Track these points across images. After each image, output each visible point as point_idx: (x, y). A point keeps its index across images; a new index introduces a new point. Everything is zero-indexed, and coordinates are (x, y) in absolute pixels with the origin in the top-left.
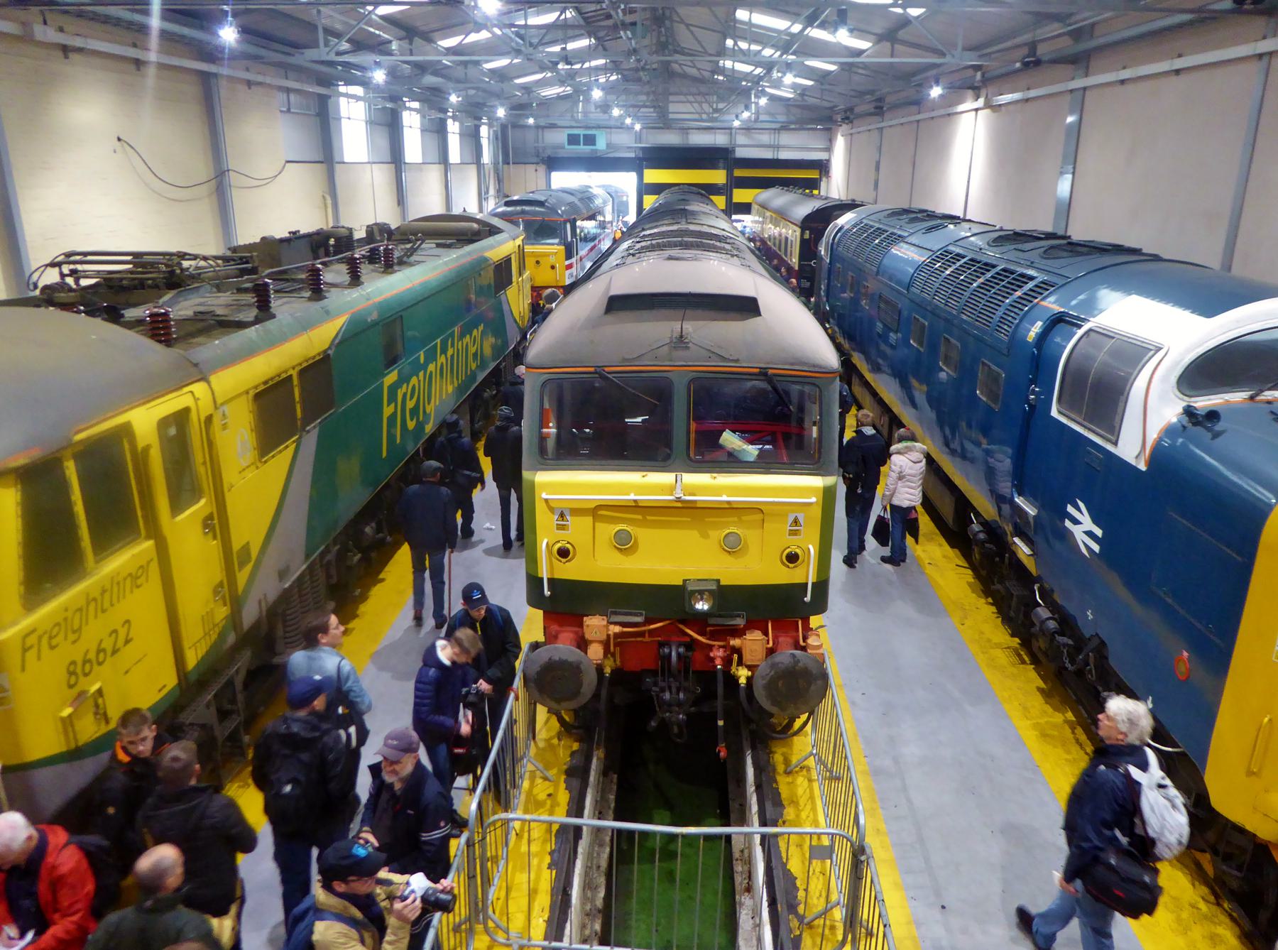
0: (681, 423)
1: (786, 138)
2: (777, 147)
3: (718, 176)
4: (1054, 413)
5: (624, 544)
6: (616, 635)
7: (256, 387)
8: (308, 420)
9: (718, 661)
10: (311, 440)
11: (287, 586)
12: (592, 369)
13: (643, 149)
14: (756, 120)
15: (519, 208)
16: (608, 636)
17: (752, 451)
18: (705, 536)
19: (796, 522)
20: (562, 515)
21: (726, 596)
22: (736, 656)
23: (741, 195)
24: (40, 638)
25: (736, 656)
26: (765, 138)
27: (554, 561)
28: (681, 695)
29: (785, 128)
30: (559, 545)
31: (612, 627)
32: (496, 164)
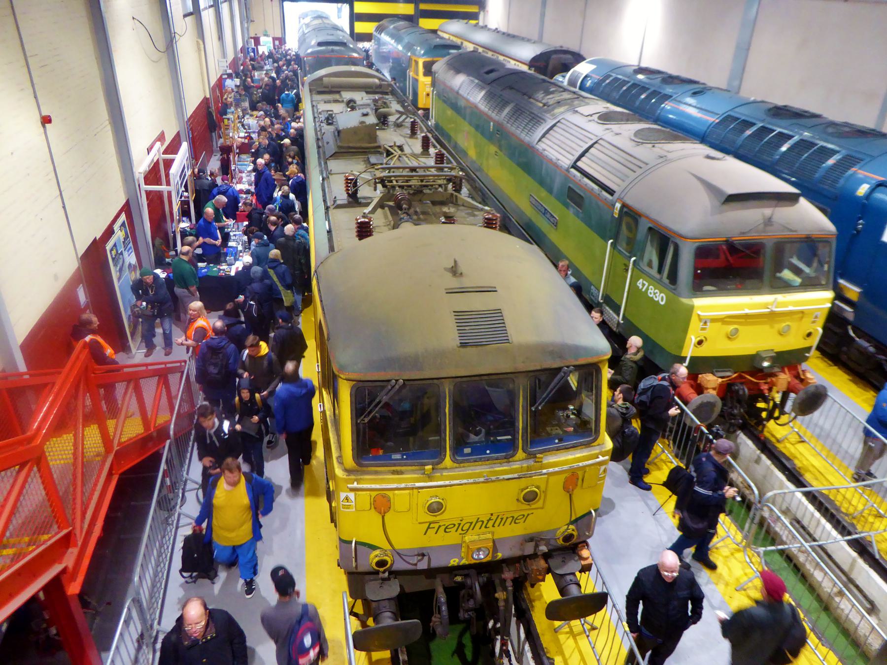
18: (772, 327)
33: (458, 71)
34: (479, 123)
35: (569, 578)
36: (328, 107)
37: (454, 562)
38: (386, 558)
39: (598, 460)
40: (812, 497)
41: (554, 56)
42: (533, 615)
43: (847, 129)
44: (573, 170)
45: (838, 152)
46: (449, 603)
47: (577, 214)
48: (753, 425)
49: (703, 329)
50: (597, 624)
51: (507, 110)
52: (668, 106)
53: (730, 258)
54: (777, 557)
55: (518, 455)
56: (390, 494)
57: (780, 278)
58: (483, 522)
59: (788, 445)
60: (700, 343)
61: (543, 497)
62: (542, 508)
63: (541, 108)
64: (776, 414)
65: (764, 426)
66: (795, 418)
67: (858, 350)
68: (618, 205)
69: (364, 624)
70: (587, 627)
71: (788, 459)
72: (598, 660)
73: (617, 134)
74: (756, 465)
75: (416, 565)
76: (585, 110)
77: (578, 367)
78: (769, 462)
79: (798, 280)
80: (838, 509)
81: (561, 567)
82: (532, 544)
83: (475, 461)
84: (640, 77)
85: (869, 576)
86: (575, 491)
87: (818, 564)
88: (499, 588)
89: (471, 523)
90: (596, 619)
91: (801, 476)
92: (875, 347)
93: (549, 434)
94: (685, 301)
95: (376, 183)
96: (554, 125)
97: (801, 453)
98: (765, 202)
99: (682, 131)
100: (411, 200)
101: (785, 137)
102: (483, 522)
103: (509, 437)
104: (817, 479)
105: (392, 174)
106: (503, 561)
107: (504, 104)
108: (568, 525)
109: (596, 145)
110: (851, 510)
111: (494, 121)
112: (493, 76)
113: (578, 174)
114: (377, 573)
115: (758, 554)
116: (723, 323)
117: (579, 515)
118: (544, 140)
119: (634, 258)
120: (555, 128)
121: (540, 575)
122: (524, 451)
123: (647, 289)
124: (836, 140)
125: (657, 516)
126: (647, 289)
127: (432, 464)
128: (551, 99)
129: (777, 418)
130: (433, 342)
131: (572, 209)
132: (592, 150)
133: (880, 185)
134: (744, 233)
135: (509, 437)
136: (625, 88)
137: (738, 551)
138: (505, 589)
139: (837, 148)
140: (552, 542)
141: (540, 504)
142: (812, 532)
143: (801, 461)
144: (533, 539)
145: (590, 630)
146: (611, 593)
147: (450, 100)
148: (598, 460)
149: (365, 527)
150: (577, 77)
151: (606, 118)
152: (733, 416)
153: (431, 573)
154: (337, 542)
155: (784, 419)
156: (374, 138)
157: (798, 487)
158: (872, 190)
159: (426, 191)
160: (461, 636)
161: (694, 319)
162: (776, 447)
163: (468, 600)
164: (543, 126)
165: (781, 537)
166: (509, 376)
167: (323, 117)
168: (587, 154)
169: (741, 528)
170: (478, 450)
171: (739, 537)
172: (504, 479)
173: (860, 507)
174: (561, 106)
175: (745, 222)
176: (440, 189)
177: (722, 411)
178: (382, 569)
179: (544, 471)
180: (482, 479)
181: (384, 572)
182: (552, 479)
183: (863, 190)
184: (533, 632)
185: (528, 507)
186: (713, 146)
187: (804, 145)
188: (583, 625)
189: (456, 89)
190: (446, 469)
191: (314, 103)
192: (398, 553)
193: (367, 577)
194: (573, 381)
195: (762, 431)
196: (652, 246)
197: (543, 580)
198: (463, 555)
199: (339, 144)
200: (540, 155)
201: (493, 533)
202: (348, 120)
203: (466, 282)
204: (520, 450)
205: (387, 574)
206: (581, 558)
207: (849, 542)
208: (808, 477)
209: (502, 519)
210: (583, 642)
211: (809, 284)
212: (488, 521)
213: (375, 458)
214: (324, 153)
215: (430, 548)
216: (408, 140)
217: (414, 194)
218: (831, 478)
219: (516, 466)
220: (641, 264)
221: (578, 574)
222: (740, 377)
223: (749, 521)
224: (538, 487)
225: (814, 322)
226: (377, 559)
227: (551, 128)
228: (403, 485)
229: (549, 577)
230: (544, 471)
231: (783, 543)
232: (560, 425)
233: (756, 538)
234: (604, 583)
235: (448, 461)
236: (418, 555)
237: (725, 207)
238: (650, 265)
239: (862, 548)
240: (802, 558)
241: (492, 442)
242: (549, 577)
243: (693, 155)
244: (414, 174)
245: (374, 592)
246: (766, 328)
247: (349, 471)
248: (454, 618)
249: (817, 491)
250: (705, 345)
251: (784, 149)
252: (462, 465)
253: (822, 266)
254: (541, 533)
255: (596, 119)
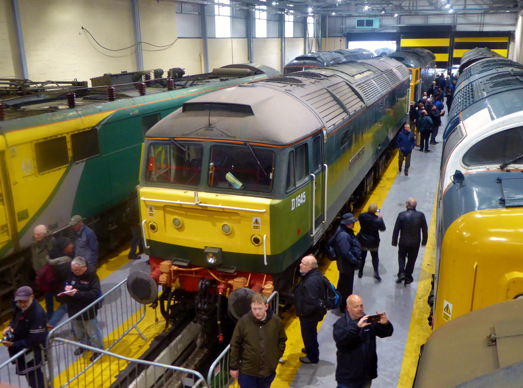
0: (209, 166)
1: (488, 19)
2: (482, 24)
3: (445, 42)
5: (179, 227)
6: (174, 271)
7: (38, 140)
8: (77, 157)
9: (221, 290)
10: (79, 168)
11: (55, 232)
12: (168, 139)
13: (400, 27)
14: (465, 9)
15: (302, 61)
16: (170, 271)
17: (239, 184)
18: (214, 225)
19: (256, 222)
20: (151, 209)
21: (224, 257)
22: (228, 289)
23: (457, 53)
25: (228, 289)
26: (475, 19)
27: (150, 231)
28: (206, 306)
29: (486, 13)
30: (151, 223)
31: (173, 267)
32: (317, 38)
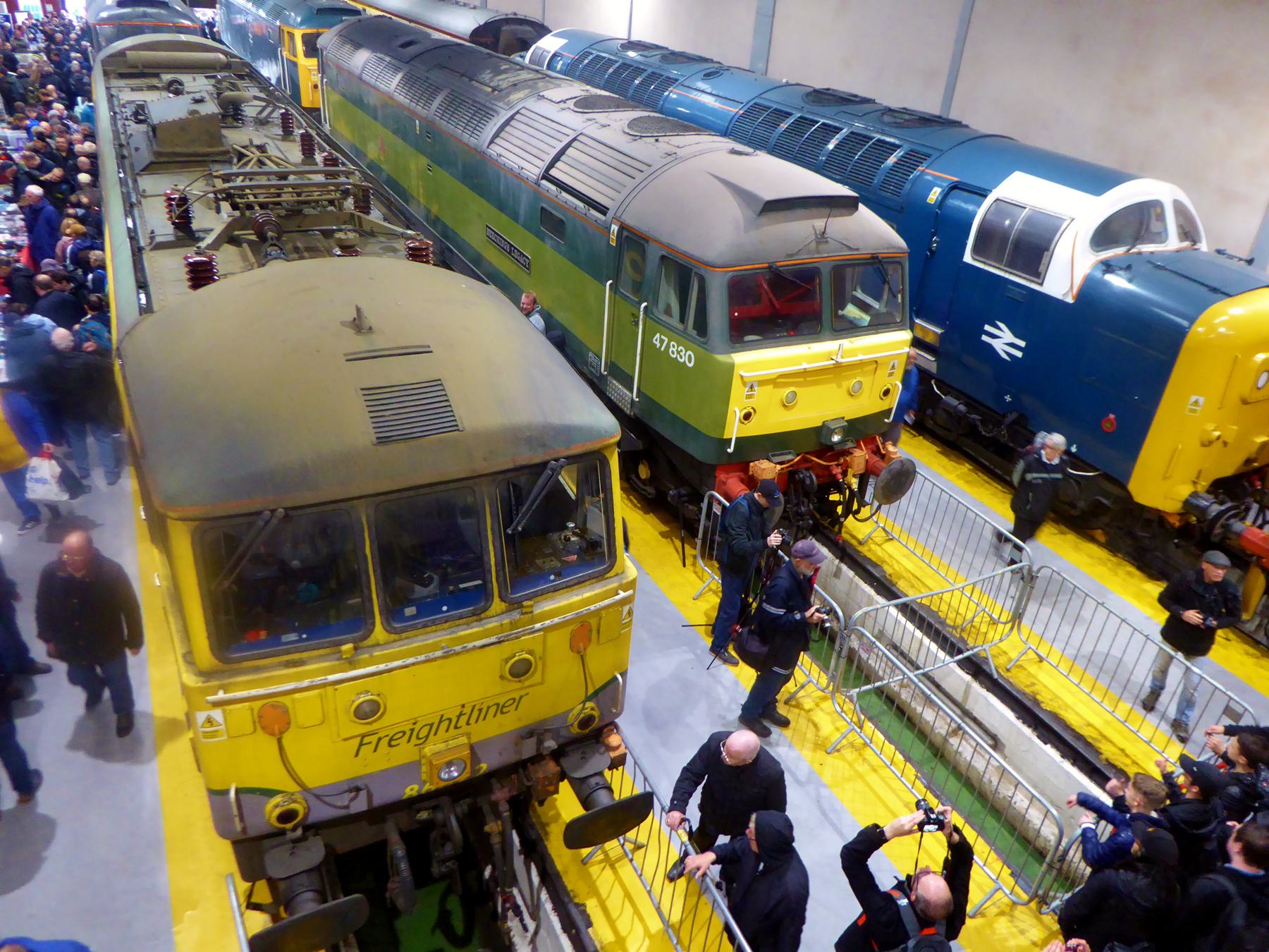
4: (968, 258)
18: (839, 386)
24: (380, 739)
33: (358, 46)
34: (400, 124)
35: (593, 781)
36: (139, 97)
37: (411, 790)
38: (293, 806)
39: (617, 598)
40: (909, 610)
41: (505, 28)
42: (549, 847)
43: (907, 117)
44: (544, 182)
45: (898, 147)
46: (411, 855)
47: (557, 248)
48: (825, 525)
49: (749, 397)
50: (642, 839)
51: (439, 100)
52: (673, 94)
53: (776, 303)
54: (874, 699)
55: (494, 606)
56: (286, 700)
57: (843, 317)
58: (450, 720)
59: (873, 546)
60: (747, 417)
61: (540, 667)
62: (542, 683)
63: (488, 94)
64: (855, 507)
65: (841, 525)
66: (879, 508)
67: (945, 410)
68: (615, 228)
69: (275, 918)
70: (629, 846)
71: (875, 565)
72: (649, 892)
73: (604, 126)
74: (836, 581)
75: (347, 807)
76: (555, 94)
77: (572, 459)
78: (851, 573)
79: (867, 319)
80: (943, 623)
81: (579, 767)
82: (534, 740)
83: (425, 626)
84: (632, 54)
85: (989, 704)
86: (589, 650)
87: (928, 698)
88: (489, 817)
89: (431, 725)
90: (640, 833)
91: (894, 585)
92: (966, 405)
93: (539, 568)
94: (722, 358)
95: (217, 200)
96: (512, 118)
97: (890, 556)
98: (814, 211)
99: (696, 123)
100: (280, 226)
101: (831, 130)
102: (450, 720)
103: (480, 582)
104: (913, 586)
105: (247, 183)
106: (490, 775)
107: (433, 91)
108: (584, 702)
109: (575, 144)
110: (959, 621)
111: (421, 118)
112: (412, 50)
113: (553, 188)
114: (282, 833)
115: (851, 699)
116: (779, 388)
117: (598, 685)
118: (497, 140)
119: (644, 304)
120: (513, 123)
121: (551, 784)
122: (502, 599)
123: (668, 346)
124: (895, 131)
125: (711, 670)
126: (668, 346)
127: (354, 641)
128: (504, 81)
129: (858, 512)
130: (330, 437)
131: (549, 242)
132: (570, 151)
133: (955, 187)
134: (791, 255)
135: (480, 582)
136: (611, 70)
137: (824, 699)
138: (498, 816)
139: (897, 142)
140: (563, 733)
141: (537, 677)
142: (914, 658)
143: (891, 566)
144: (534, 732)
145: (633, 851)
146: (656, 790)
147: (356, 97)
148: (617, 598)
149: (257, 765)
150: (542, 57)
151: (585, 104)
152: (800, 515)
153: (376, 815)
154: (204, 794)
155: (866, 512)
156: (219, 139)
157: (889, 600)
158: (945, 196)
159: (307, 211)
160: (443, 900)
161: (736, 382)
162: (858, 552)
163: (443, 845)
164: (495, 120)
165: (876, 673)
166: (465, 483)
167: (129, 111)
168: (563, 158)
169: (825, 668)
170: (428, 610)
171: (824, 680)
172: (474, 648)
173: (969, 616)
174: (519, 90)
175: (796, 233)
176: (331, 208)
177: (785, 511)
178: (289, 826)
179: (538, 626)
180: (439, 653)
181: (294, 829)
182: (553, 638)
183: (934, 195)
184: (550, 871)
185: (518, 685)
186: (737, 139)
187: (857, 139)
188: (623, 846)
189: (358, 72)
190: (378, 645)
191: (113, 92)
192: (318, 797)
193: (266, 843)
194: (570, 486)
195: (840, 531)
196: (668, 282)
197: (556, 792)
198: (424, 777)
199: (156, 148)
200: (495, 163)
201: (468, 735)
202: (165, 108)
203: (379, 342)
204: (496, 599)
205: (299, 832)
206: (610, 748)
207: (961, 664)
208: (902, 585)
209: (480, 710)
210: (625, 870)
211: (879, 324)
212: (459, 717)
213: (252, 646)
214: (132, 166)
215: (367, 776)
216: (280, 143)
217: (287, 217)
218: (929, 582)
219: (492, 624)
220: (655, 311)
221: (607, 773)
222: (804, 460)
223: (834, 655)
224: (530, 652)
225: (891, 374)
226: (278, 811)
227: (507, 123)
228: (306, 683)
229: (565, 786)
230: (538, 626)
231: (881, 679)
232: (556, 554)
233: (846, 679)
234: (646, 779)
235: (379, 633)
236: (350, 791)
237: (764, 219)
238: (668, 311)
239: (976, 668)
240: (905, 695)
241: (452, 592)
242: (565, 786)
243: (712, 154)
244: (283, 182)
245: (280, 863)
246: (832, 387)
247: (206, 675)
248: (422, 877)
249: (914, 601)
250: (754, 419)
251: (831, 146)
252: (404, 635)
253: (895, 297)
254: (544, 721)
255: (572, 107)
